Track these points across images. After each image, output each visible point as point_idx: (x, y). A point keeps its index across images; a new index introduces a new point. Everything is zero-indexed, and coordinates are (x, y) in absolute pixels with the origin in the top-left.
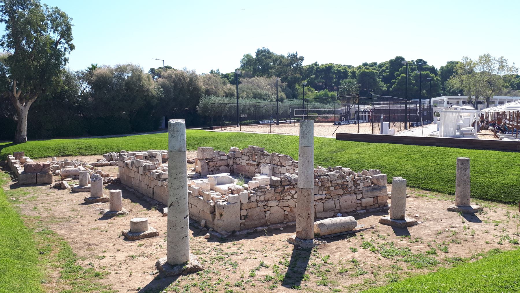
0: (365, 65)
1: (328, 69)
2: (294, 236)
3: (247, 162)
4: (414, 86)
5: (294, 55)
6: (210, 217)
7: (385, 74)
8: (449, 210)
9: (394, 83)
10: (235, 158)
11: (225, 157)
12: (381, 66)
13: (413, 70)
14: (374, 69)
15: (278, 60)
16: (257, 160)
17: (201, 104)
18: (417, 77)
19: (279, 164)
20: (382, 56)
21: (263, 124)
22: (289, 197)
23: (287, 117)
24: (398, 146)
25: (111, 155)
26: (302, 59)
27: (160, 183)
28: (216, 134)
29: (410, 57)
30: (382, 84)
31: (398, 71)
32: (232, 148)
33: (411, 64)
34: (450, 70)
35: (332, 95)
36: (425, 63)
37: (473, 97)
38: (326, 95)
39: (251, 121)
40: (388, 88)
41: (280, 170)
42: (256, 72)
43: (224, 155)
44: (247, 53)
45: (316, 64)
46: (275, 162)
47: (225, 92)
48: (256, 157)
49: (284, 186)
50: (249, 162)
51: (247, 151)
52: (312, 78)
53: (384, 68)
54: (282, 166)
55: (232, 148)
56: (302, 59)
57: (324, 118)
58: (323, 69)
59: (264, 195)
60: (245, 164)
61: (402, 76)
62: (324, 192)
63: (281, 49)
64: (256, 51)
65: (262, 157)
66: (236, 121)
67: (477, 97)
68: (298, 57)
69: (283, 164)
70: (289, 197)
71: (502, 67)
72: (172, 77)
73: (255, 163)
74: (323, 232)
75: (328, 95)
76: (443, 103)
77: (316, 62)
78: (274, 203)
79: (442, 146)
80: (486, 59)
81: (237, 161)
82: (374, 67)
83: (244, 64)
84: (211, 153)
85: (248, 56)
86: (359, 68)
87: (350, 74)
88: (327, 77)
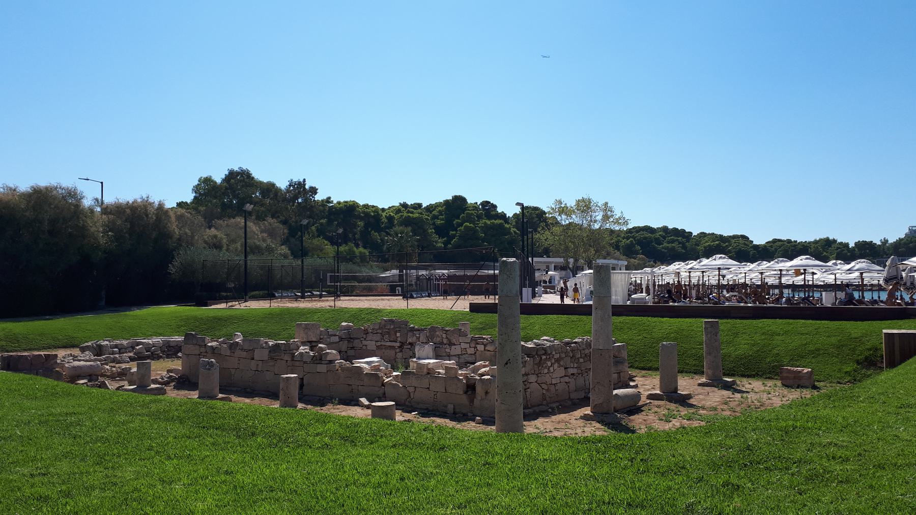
0: (404, 205)
1: (349, 210)
2: (587, 411)
3: (379, 344)
4: (483, 242)
5: (299, 183)
6: (464, 399)
7: (439, 222)
8: (700, 385)
9: (454, 236)
10: (350, 339)
11: (336, 339)
12: (430, 208)
13: (479, 217)
14: (421, 213)
15: (269, 189)
16: (399, 339)
17: (177, 262)
18: (486, 228)
19: (445, 341)
20: (431, 194)
21: (282, 297)
22: (546, 371)
23: (313, 287)
24: (574, 318)
25: (100, 346)
26: (314, 191)
27: (322, 368)
28: (212, 314)
29: (474, 198)
30: (435, 237)
31: (458, 218)
32: (344, 324)
33: (475, 207)
34: (531, 218)
35: (360, 253)
36: (495, 207)
37: (571, 261)
38: (351, 252)
39: (261, 293)
40: (446, 244)
41: (448, 350)
42: (227, 211)
43: (335, 335)
44: (205, 176)
45: (328, 200)
46: (438, 339)
47: (206, 242)
48: (398, 335)
49: (540, 356)
50: (383, 343)
51: (377, 327)
52: (322, 224)
53: (435, 213)
54: (451, 344)
55: (344, 324)
56: (314, 191)
57: (365, 288)
58: (341, 208)
59: (524, 366)
60: (374, 348)
61: (466, 226)
62: (576, 365)
63: (276, 173)
64: (227, 173)
65: (410, 334)
66: (243, 292)
67: (576, 261)
68: (307, 187)
69: (454, 341)
70: (546, 371)
71: (606, 218)
72: (125, 211)
73: (398, 344)
74: (619, 404)
75: (354, 252)
76: (555, 267)
77: (329, 198)
78: (533, 378)
79: (245, 397)
80: (585, 206)
81: (356, 343)
82: (419, 211)
83: (200, 194)
84: (318, 332)
85: (207, 181)
86: (398, 211)
87: (384, 220)
88: (352, 222)
